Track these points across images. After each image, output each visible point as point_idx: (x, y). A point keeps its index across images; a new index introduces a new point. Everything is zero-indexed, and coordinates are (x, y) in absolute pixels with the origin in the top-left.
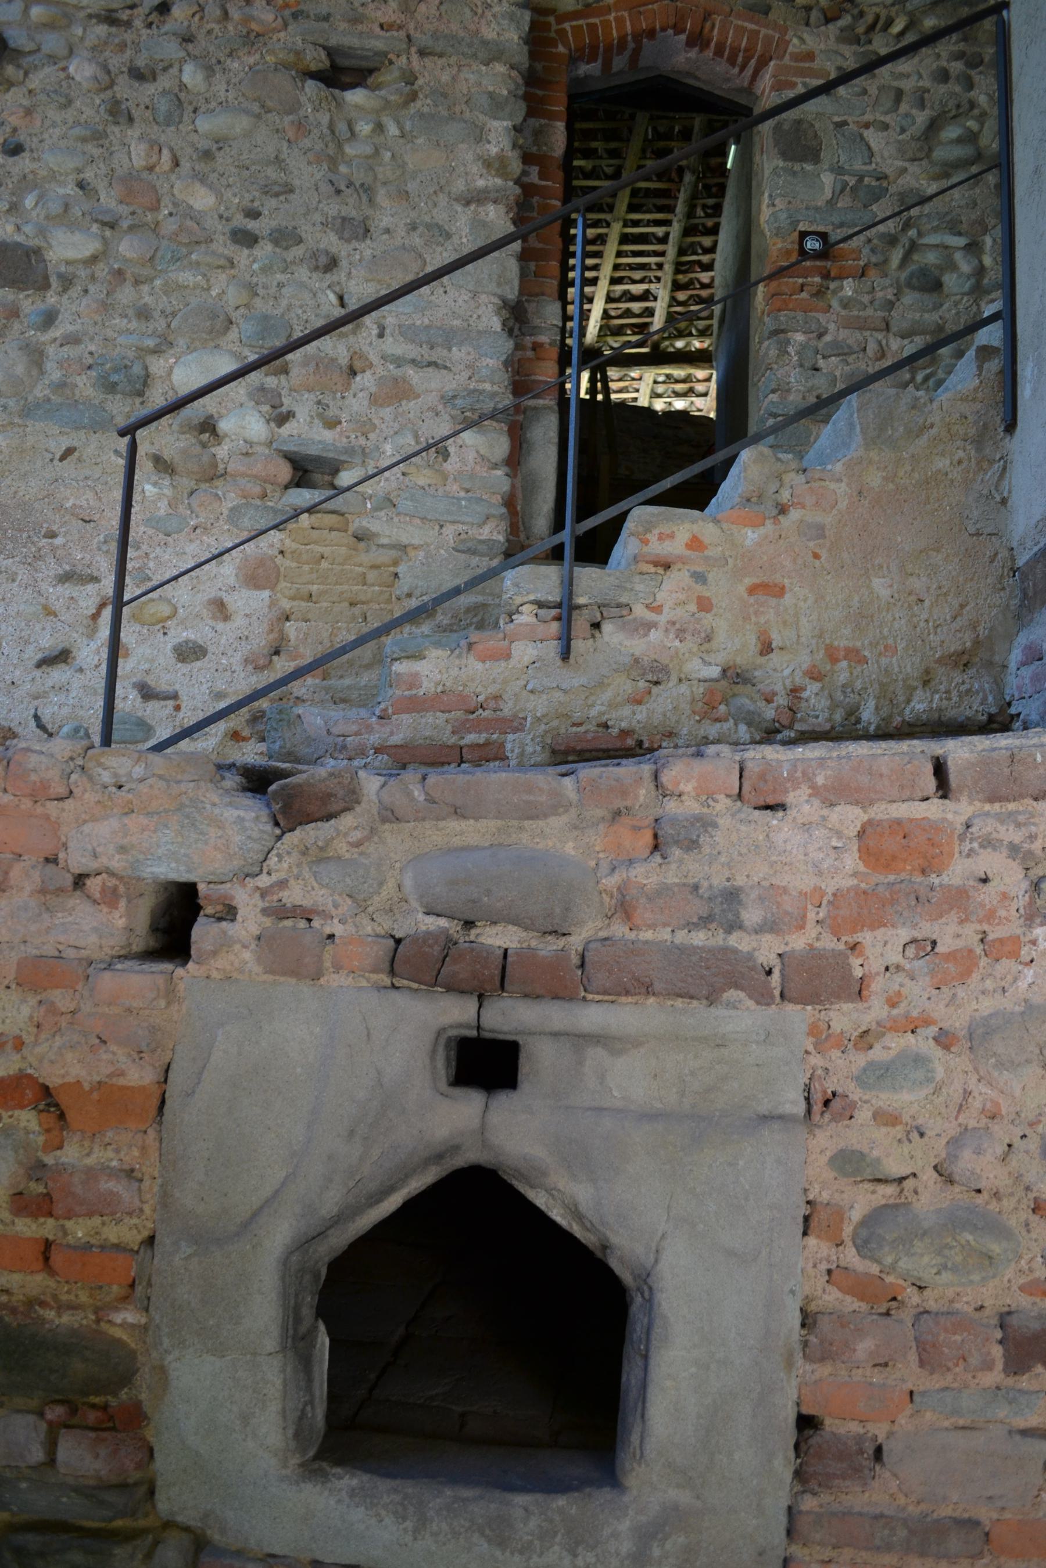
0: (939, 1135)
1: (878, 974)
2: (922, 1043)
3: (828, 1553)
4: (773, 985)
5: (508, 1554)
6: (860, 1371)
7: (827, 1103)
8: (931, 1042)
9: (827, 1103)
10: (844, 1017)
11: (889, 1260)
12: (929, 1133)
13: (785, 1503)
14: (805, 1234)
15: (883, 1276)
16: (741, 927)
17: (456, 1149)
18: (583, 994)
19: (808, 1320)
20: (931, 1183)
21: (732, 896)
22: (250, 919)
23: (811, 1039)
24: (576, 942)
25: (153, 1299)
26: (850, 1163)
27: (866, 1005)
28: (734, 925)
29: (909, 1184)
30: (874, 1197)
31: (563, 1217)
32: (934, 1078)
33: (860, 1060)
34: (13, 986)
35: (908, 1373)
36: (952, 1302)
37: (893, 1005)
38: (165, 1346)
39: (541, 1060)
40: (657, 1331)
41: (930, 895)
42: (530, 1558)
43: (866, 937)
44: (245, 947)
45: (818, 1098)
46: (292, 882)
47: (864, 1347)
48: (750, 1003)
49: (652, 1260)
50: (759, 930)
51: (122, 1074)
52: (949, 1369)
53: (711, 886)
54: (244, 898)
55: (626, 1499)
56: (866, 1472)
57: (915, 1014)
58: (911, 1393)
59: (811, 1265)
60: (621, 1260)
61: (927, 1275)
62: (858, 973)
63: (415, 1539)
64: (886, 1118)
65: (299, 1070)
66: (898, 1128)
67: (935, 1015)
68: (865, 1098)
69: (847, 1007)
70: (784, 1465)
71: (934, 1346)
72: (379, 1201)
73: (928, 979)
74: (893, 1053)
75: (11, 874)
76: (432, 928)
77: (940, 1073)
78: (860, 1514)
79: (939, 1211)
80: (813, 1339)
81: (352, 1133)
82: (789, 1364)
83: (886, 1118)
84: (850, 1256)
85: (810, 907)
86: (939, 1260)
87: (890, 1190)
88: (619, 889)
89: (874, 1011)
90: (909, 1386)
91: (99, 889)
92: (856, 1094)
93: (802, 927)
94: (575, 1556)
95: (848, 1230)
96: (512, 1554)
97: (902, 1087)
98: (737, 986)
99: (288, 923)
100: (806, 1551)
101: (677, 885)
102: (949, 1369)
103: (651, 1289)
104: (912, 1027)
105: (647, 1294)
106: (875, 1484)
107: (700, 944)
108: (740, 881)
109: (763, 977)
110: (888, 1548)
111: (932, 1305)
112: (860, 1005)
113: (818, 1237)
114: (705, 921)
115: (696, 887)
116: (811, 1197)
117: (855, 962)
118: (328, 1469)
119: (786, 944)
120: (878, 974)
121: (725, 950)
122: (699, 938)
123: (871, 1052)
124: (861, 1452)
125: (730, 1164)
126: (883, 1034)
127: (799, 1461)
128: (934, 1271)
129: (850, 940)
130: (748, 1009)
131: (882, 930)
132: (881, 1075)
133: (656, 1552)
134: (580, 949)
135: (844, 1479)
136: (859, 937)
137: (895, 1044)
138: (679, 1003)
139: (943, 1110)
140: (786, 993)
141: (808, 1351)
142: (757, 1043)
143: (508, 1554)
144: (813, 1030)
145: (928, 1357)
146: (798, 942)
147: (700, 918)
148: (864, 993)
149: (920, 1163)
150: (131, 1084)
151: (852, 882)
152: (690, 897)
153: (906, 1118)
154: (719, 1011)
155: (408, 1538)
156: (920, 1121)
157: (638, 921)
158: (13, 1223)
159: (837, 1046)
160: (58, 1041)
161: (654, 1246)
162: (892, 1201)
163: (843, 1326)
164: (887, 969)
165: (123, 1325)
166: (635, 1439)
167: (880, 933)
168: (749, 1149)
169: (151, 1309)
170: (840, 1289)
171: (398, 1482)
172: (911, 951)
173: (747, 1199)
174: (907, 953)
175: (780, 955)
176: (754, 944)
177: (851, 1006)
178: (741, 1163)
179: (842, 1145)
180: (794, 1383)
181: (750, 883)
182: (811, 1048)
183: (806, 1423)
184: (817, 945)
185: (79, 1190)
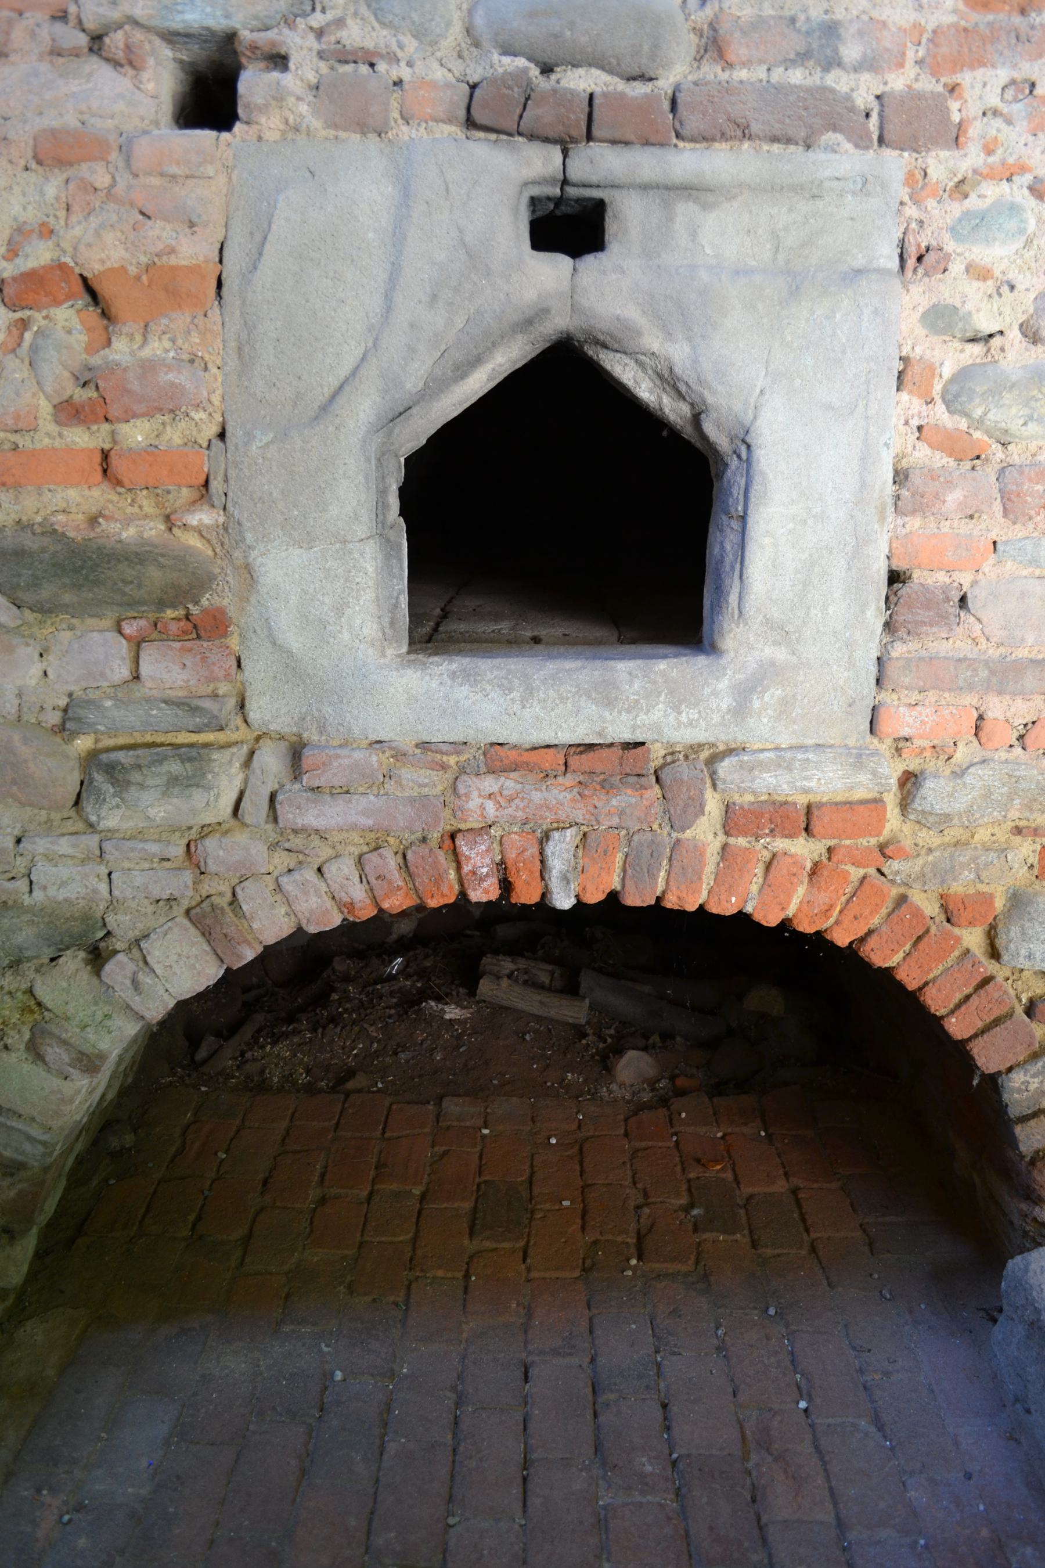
0: (1027, 290)
1: (975, 118)
2: (1018, 192)
3: (915, 696)
4: (872, 128)
5: (615, 713)
6: (948, 523)
7: (920, 259)
8: (1026, 192)
9: (920, 259)
10: (941, 165)
11: (978, 412)
12: (1019, 287)
13: (875, 654)
14: (898, 390)
15: (971, 431)
16: (840, 64)
17: (543, 312)
18: (675, 141)
19: (900, 477)
20: (1016, 342)
21: (831, 30)
22: (306, 65)
23: (907, 190)
24: (665, 84)
25: (230, 494)
26: (941, 319)
27: (962, 152)
28: (833, 62)
29: (996, 342)
30: (962, 356)
31: (651, 392)
32: (1025, 229)
33: (956, 208)
34: (33, 165)
35: (993, 524)
36: (1034, 455)
37: (989, 152)
38: (248, 542)
39: (629, 218)
40: (756, 488)
41: (1031, 33)
42: (637, 716)
43: (965, 77)
44: (299, 99)
45: (912, 253)
46: (350, 22)
47: (953, 498)
48: (848, 146)
49: (751, 416)
50: (857, 68)
51: (172, 251)
52: (1031, 518)
53: (808, 19)
54: (299, 44)
55: (723, 661)
56: (952, 618)
57: (1011, 160)
58: (995, 543)
59: (902, 422)
60: (718, 425)
61: (1015, 426)
62: (956, 117)
63: (524, 707)
64: (978, 272)
65: (371, 235)
66: (990, 283)
67: (1031, 163)
68: (959, 251)
69: (944, 154)
70: (875, 617)
71: (1018, 495)
72: (463, 376)
73: (1025, 123)
74: (988, 201)
75: (13, 36)
76: (510, 69)
77: (1032, 226)
78: (946, 658)
79: (1024, 367)
80: (905, 493)
81: (434, 297)
82: (882, 518)
83: (978, 272)
84: (940, 413)
85: (909, 44)
86: (1026, 411)
87: (977, 349)
88: (711, 24)
89: (971, 159)
90: (993, 536)
91: (121, 45)
92: (950, 246)
93: (901, 65)
94: (680, 713)
95: (938, 387)
96: (620, 713)
97: (995, 239)
98: (835, 129)
99: (349, 68)
100: (895, 696)
101: (773, 17)
102: (1031, 518)
103: (749, 447)
104: (1008, 174)
105: (744, 455)
106: (959, 630)
107: (798, 82)
108: (839, 14)
109: (862, 119)
110: (971, 687)
111: (1016, 459)
112: (957, 153)
113: (910, 392)
114: (802, 58)
115: (793, 20)
116: (904, 354)
117: (954, 105)
118: (425, 659)
119: (886, 83)
120: (975, 118)
121: (824, 89)
122: (797, 76)
123: (967, 201)
124: (948, 600)
125: (828, 318)
126: (979, 183)
127: (889, 612)
128: (1021, 422)
129: (949, 81)
130: (846, 152)
131: (982, 70)
132: (977, 225)
133: (756, 704)
134: (670, 92)
135: (932, 626)
136: (957, 78)
137: (992, 192)
138: (776, 148)
139: (1033, 265)
140: (887, 137)
141: (900, 503)
142: (854, 193)
143: (615, 713)
144: (909, 179)
145: (1011, 506)
146: (897, 82)
147: (798, 54)
148: (962, 139)
149: (1008, 320)
150: (184, 263)
151: (952, 19)
152: (786, 31)
153: (997, 273)
154: (817, 156)
155: (516, 707)
156: (1010, 276)
157: (731, 57)
158: (60, 435)
159: (934, 195)
160: (94, 221)
161: (752, 401)
162: (978, 361)
163: (933, 479)
164: (984, 114)
165: (199, 531)
166: (733, 599)
167: (980, 73)
168: (846, 301)
169: (229, 506)
170: (930, 446)
171: (499, 660)
172: (1009, 94)
173: (844, 352)
174: (1006, 96)
175: (878, 97)
176: (852, 84)
177: (947, 153)
178: (838, 316)
179: (934, 300)
180: (886, 537)
181: (849, 17)
182: (906, 199)
183: (895, 578)
184: (916, 86)
185: (135, 386)
